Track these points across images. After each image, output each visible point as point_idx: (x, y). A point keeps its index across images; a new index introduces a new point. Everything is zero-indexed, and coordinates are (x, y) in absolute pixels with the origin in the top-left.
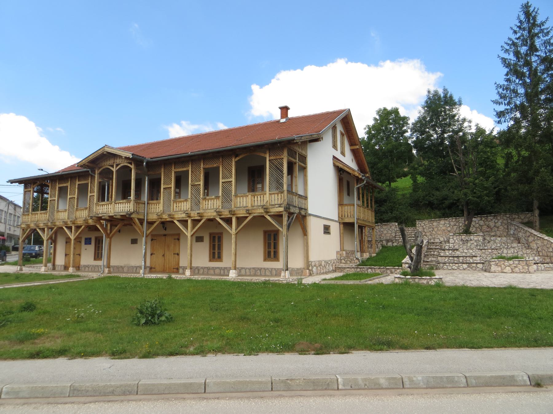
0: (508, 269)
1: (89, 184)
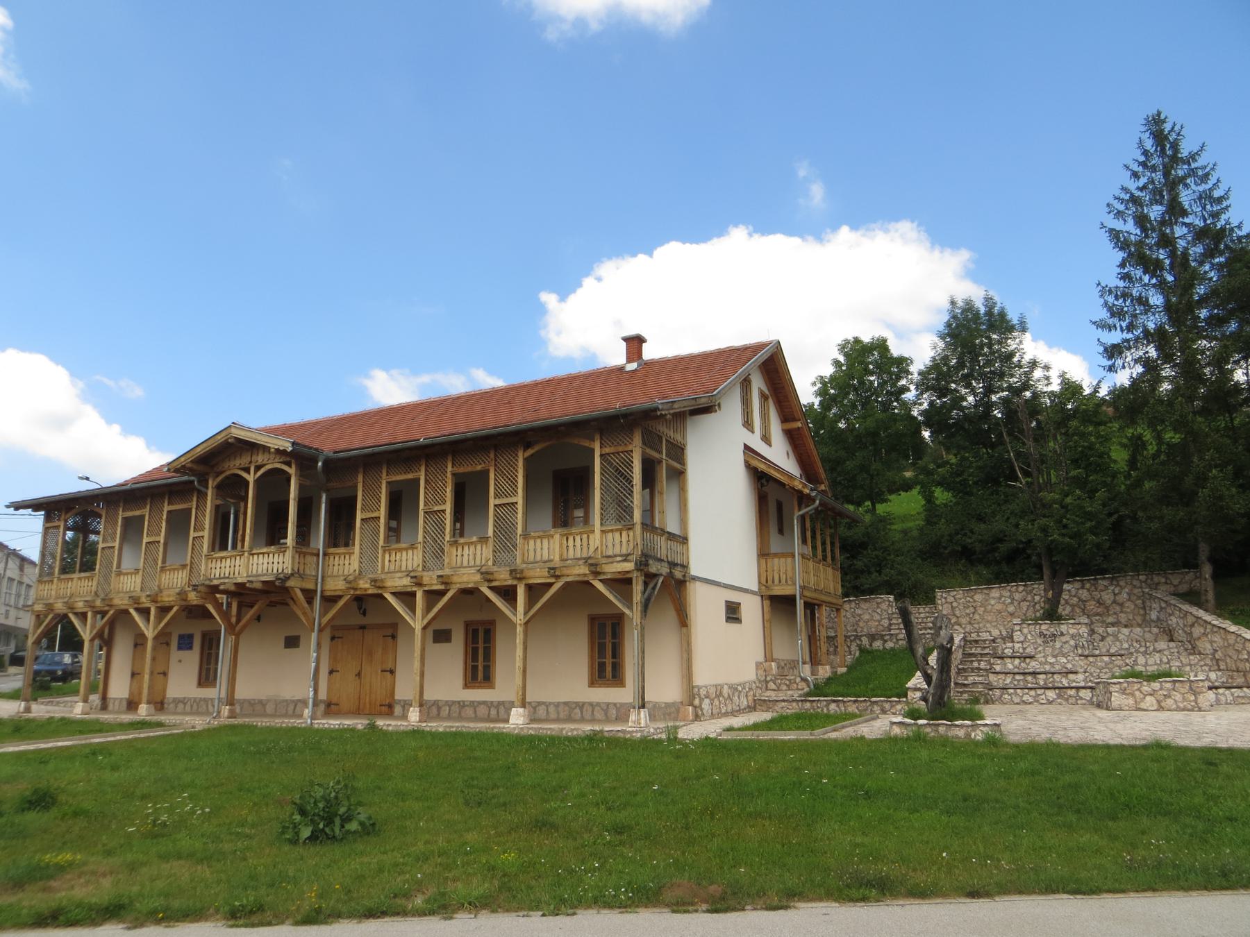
0: (1150, 701)
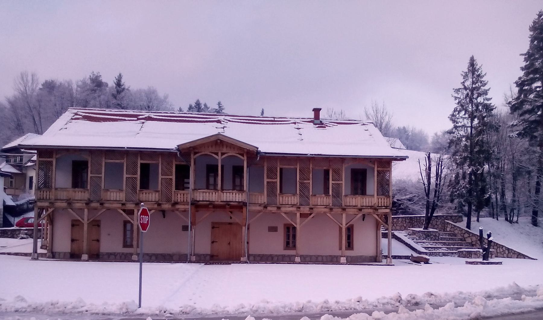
1: (125, 165)
